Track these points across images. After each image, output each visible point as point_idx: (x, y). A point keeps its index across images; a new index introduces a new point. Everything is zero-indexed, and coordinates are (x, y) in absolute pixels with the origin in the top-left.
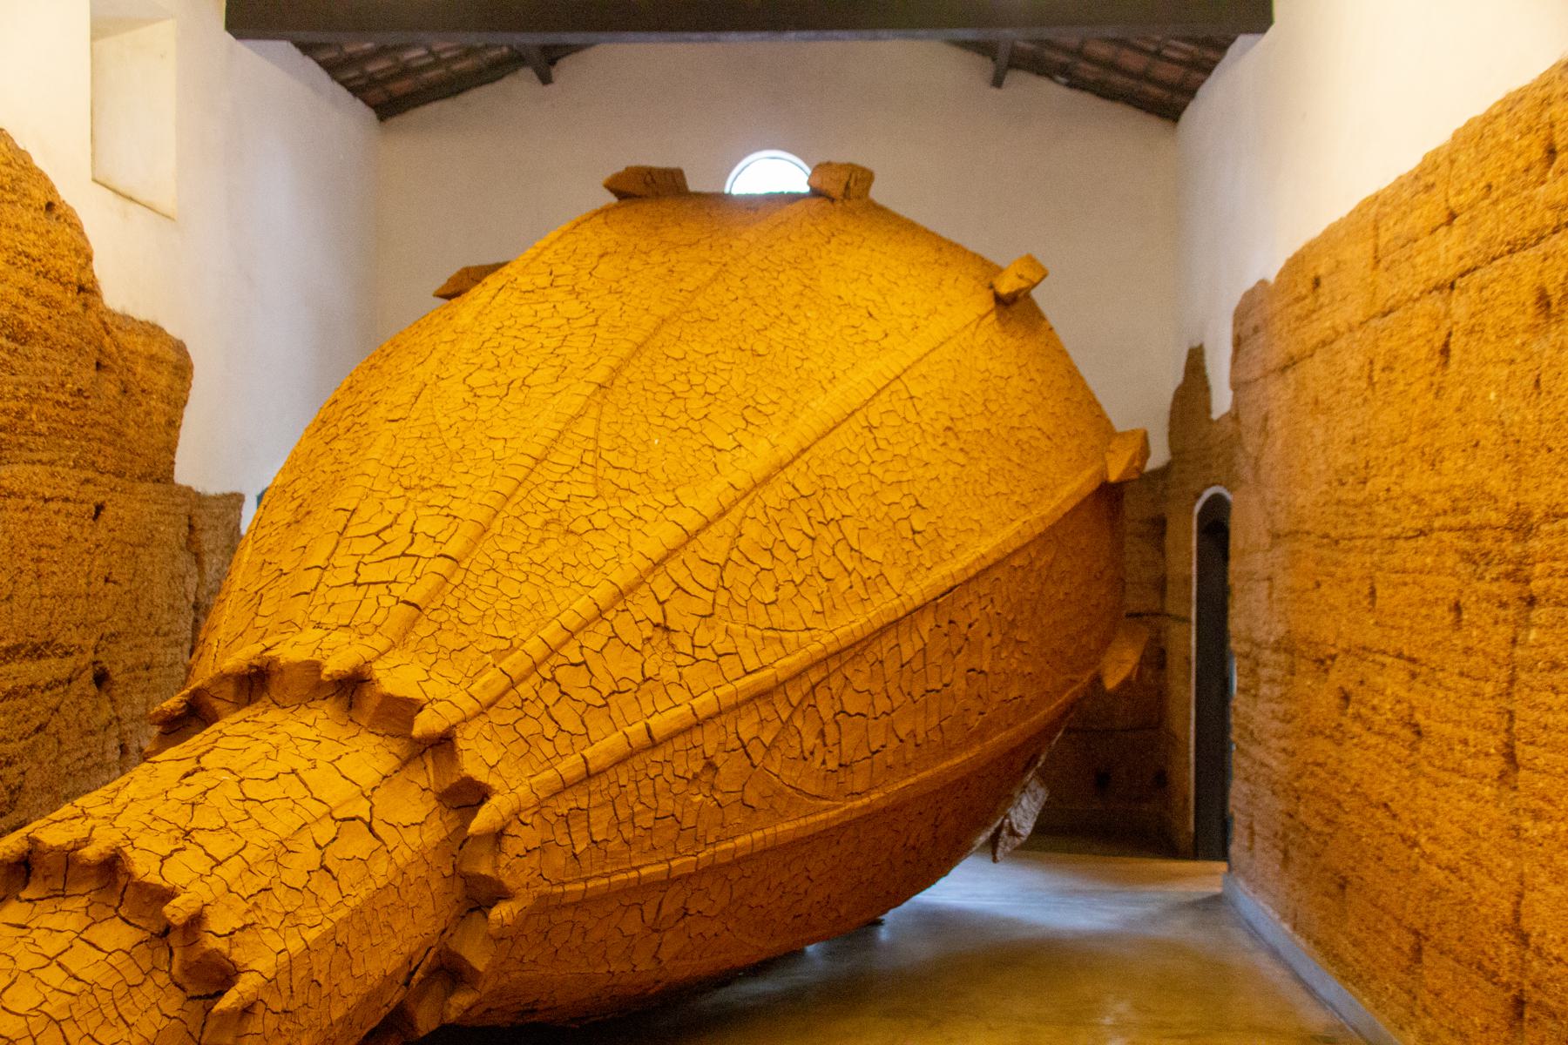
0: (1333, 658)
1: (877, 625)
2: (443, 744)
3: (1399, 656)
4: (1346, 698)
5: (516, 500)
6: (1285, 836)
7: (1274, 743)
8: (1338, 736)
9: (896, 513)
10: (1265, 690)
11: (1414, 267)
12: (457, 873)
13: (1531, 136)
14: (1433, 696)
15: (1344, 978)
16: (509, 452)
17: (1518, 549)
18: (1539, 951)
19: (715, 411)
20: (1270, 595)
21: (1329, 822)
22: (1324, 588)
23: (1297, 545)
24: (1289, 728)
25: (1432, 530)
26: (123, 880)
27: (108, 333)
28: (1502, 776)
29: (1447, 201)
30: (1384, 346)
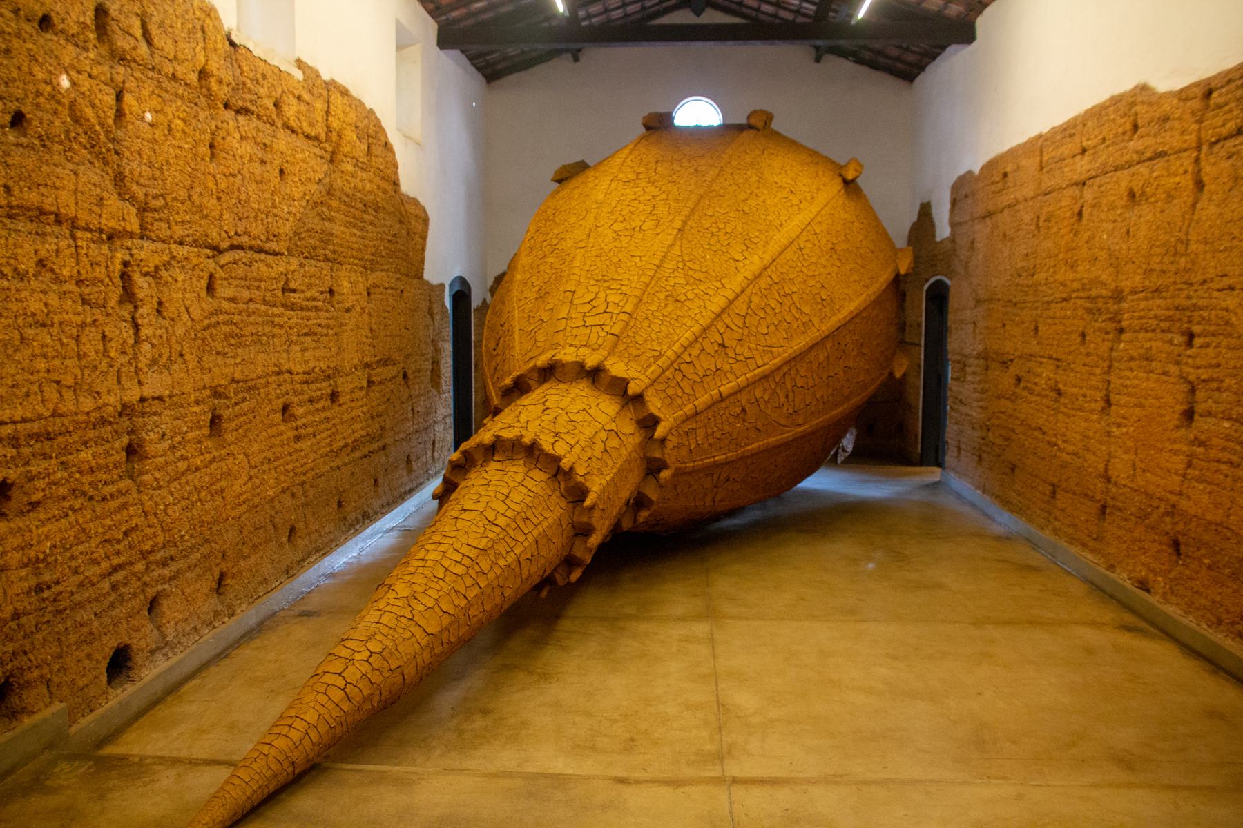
0: (1012, 361)
2: (639, 399)
3: (1050, 358)
4: (1019, 379)
7: (975, 404)
8: (1013, 398)
10: (969, 378)
12: (645, 457)
13: (1125, 119)
15: (1011, 511)
17: (1115, 307)
18: (1115, 484)
20: (974, 331)
21: (1007, 439)
24: (984, 396)
25: (1071, 298)
26: (537, 453)
28: (1103, 409)
30: (1046, 210)
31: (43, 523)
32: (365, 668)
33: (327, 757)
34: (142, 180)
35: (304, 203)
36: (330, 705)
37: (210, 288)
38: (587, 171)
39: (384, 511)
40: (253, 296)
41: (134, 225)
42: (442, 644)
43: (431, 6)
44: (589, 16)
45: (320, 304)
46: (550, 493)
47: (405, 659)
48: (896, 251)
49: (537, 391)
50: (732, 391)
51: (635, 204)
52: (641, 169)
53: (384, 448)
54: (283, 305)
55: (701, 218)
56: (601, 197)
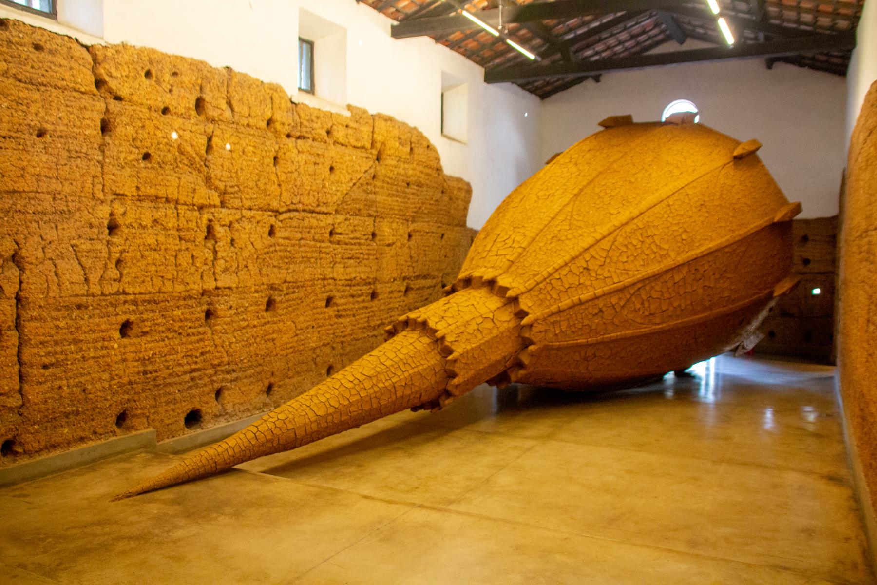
2: (515, 300)
9: (676, 234)
12: (519, 336)
31: (149, 342)
34: (222, 179)
37: (271, 233)
41: (217, 202)
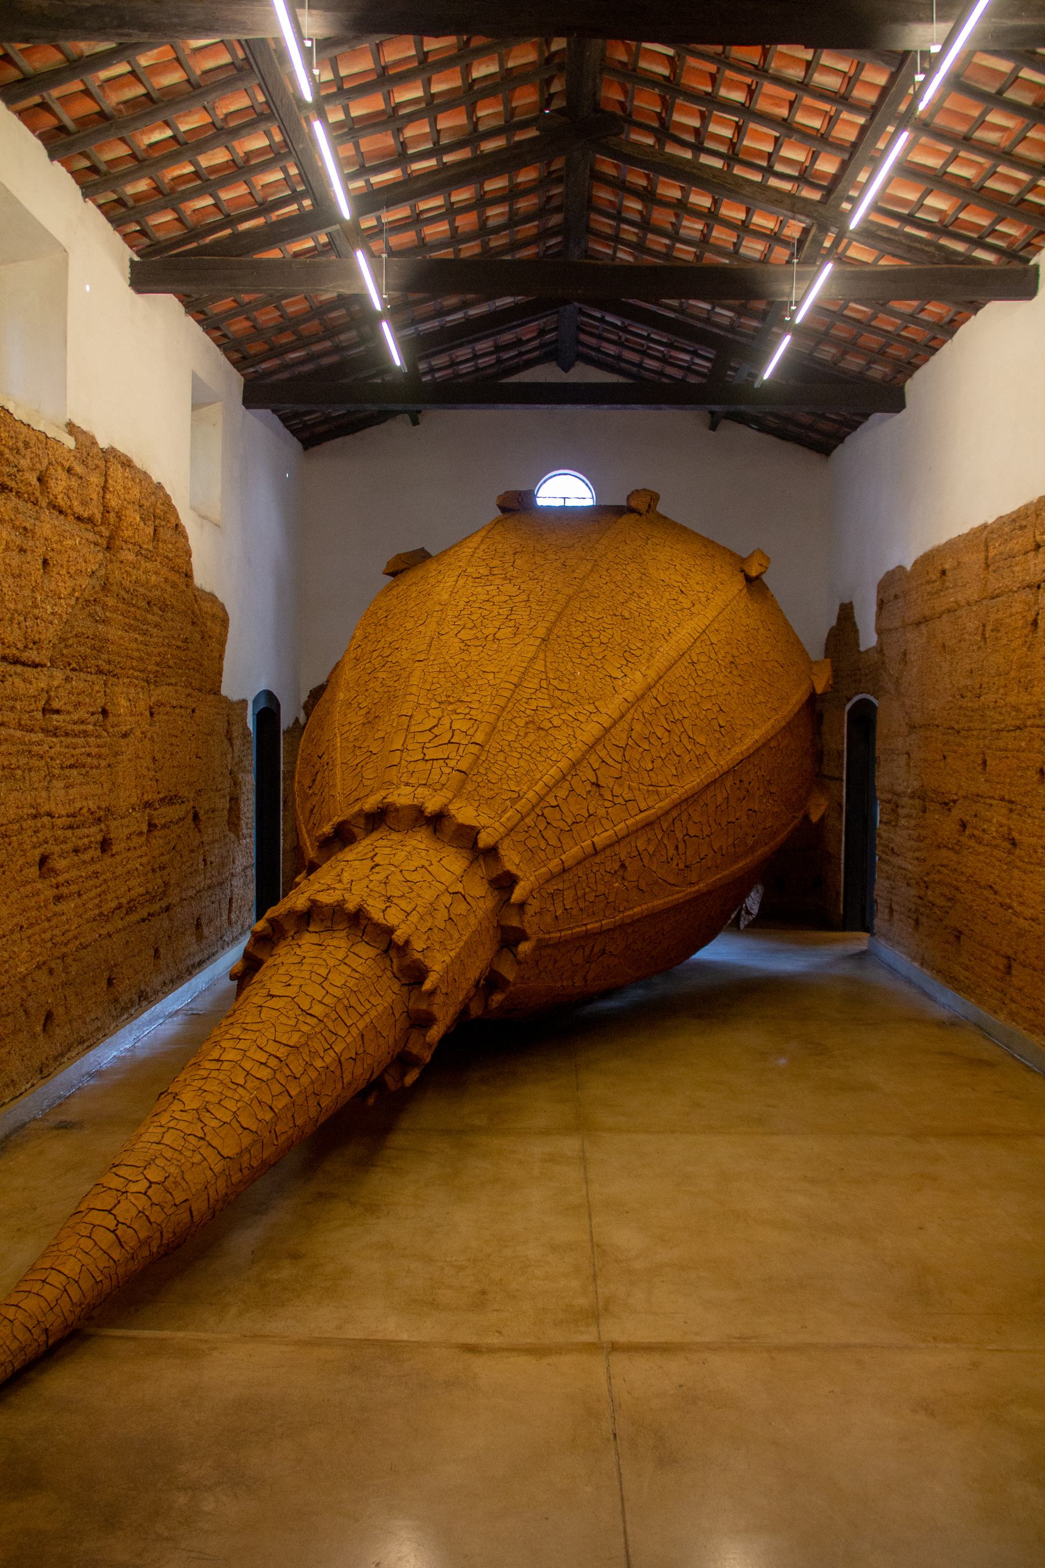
1: (706, 783)
2: (492, 853)
3: (1002, 799)
4: (964, 825)
5: (508, 709)
6: (917, 910)
7: (910, 854)
9: (710, 716)
10: (903, 822)
11: (1013, 572)
14: (1024, 822)
15: (957, 990)
16: (498, 681)
19: (609, 655)
20: (908, 764)
21: (950, 899)
22: (949, 760)
23: (928, 734)
24: (921, 844)
25: (1026, 727)
26: (364, 922)
27: (196, 601)
29: (1034, 537)
30: (993, 617)
32: (142, 1202)
33: (90, 1318)
35: (73, 602)
36: (96, 1253)
38: (428, 562)
39: (165, 989)
40: (5, 719)
42: (241, 1170)
43: (236, 356)
44: (432, 370)
45: (90, 727)
46: (380, 974)
47: (194, 1191)
48: (811, 664)
49: (364, 843)
50: (608, 842)
51: (488, 606)
52: (496, 562)
53: (168, 909)
54: (43, 730)
55: (569, 625)
56: (445, 596)
